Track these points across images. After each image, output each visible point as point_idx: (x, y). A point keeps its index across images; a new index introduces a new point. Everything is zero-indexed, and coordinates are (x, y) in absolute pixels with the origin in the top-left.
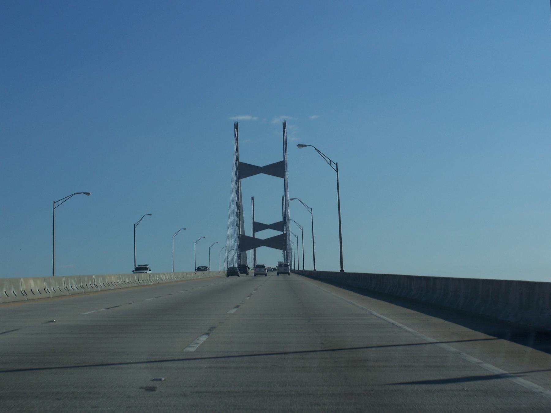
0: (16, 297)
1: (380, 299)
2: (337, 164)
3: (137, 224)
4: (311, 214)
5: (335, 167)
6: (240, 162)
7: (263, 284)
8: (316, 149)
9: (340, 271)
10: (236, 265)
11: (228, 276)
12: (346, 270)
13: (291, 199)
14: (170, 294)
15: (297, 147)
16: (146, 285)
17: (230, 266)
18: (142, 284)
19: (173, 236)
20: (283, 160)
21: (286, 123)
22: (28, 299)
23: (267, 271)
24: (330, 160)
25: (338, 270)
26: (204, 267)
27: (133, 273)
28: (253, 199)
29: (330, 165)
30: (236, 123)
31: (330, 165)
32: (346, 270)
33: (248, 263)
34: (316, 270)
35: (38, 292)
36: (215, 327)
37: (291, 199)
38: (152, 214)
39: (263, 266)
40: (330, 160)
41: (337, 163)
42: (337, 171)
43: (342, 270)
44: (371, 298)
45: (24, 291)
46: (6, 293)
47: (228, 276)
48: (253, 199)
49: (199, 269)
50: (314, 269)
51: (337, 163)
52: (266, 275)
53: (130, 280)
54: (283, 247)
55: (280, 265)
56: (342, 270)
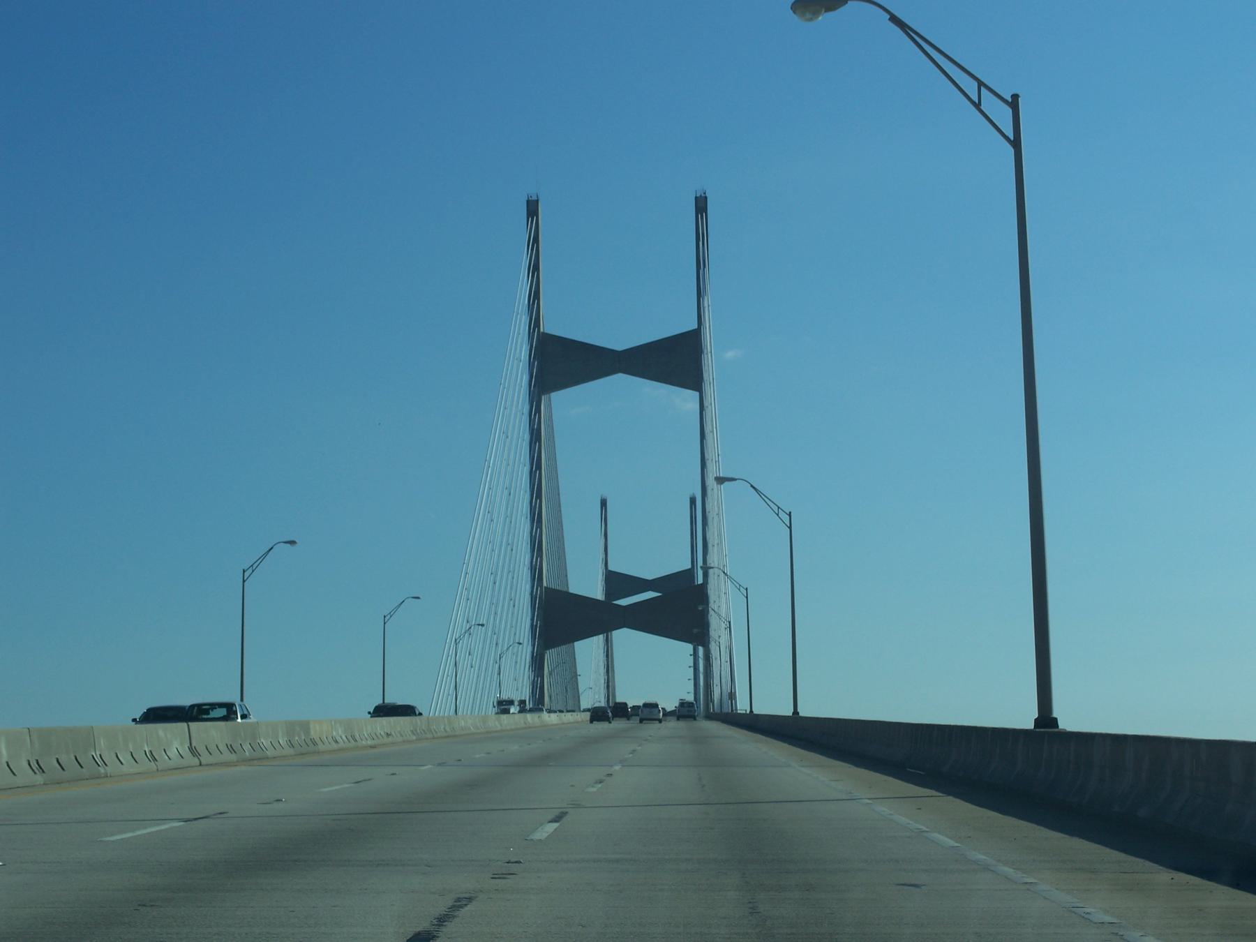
0: (83, 770)
1: (811, 751)
2: (790, 515)
3: (389, 616)
4: (746, 599)
5: (1003, 116)
6: (543, 333)
7: (650, 738)
8: (752, 486)
9: (791, 714)
10: (603, 704)
11: (591, 722)
12: (1070, 718)
13: (720, 480)
14: (460, 760)
15: (795, 17)
16: (580, 720)
17: (628, 703)
18: (435, 735)
19: (385, 617)
20: (696, 327)
21: (706, 198)
22: (204, 762)
23: (663, 715)
24: (779, 508)
25: (789, 712)
26: (221, 705)
27: (371, 717)
28: (604, 503)
29: (778, 515)
30: (534, 198)
31: (778, 515)
32: (804, 712)
33: (580, 691)
34: (801, 714)
35: (57, 765)
36: (470, 899)
37: (720, 480)
38: (421, 597)
39: (656, 706)
40: (779, 508)
41: (1015, 97)
42: (790, 528)
43: (796, 712)
44: (963, 802)
45: (98, 756)
46: (40, 763)
47: (591, 722)
48: (604, 503)
49: (383, 710)
50: (751, 711)
51: (1015, 97)
52: (660, 721)
53: (303, 738)
54: (695, 631)
55: (683, 704)
56: (796, 712)
